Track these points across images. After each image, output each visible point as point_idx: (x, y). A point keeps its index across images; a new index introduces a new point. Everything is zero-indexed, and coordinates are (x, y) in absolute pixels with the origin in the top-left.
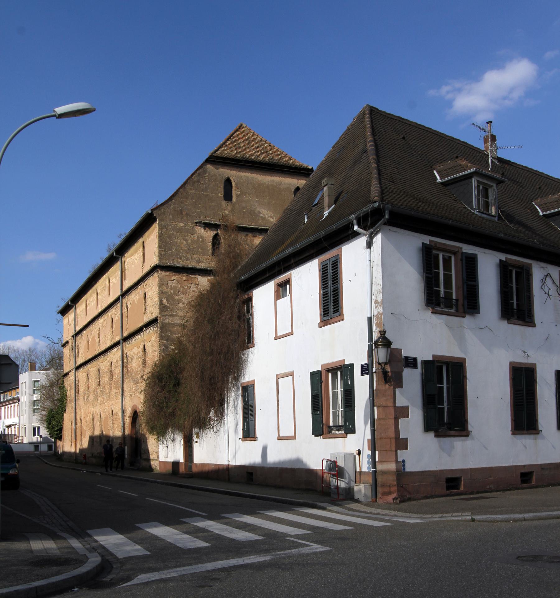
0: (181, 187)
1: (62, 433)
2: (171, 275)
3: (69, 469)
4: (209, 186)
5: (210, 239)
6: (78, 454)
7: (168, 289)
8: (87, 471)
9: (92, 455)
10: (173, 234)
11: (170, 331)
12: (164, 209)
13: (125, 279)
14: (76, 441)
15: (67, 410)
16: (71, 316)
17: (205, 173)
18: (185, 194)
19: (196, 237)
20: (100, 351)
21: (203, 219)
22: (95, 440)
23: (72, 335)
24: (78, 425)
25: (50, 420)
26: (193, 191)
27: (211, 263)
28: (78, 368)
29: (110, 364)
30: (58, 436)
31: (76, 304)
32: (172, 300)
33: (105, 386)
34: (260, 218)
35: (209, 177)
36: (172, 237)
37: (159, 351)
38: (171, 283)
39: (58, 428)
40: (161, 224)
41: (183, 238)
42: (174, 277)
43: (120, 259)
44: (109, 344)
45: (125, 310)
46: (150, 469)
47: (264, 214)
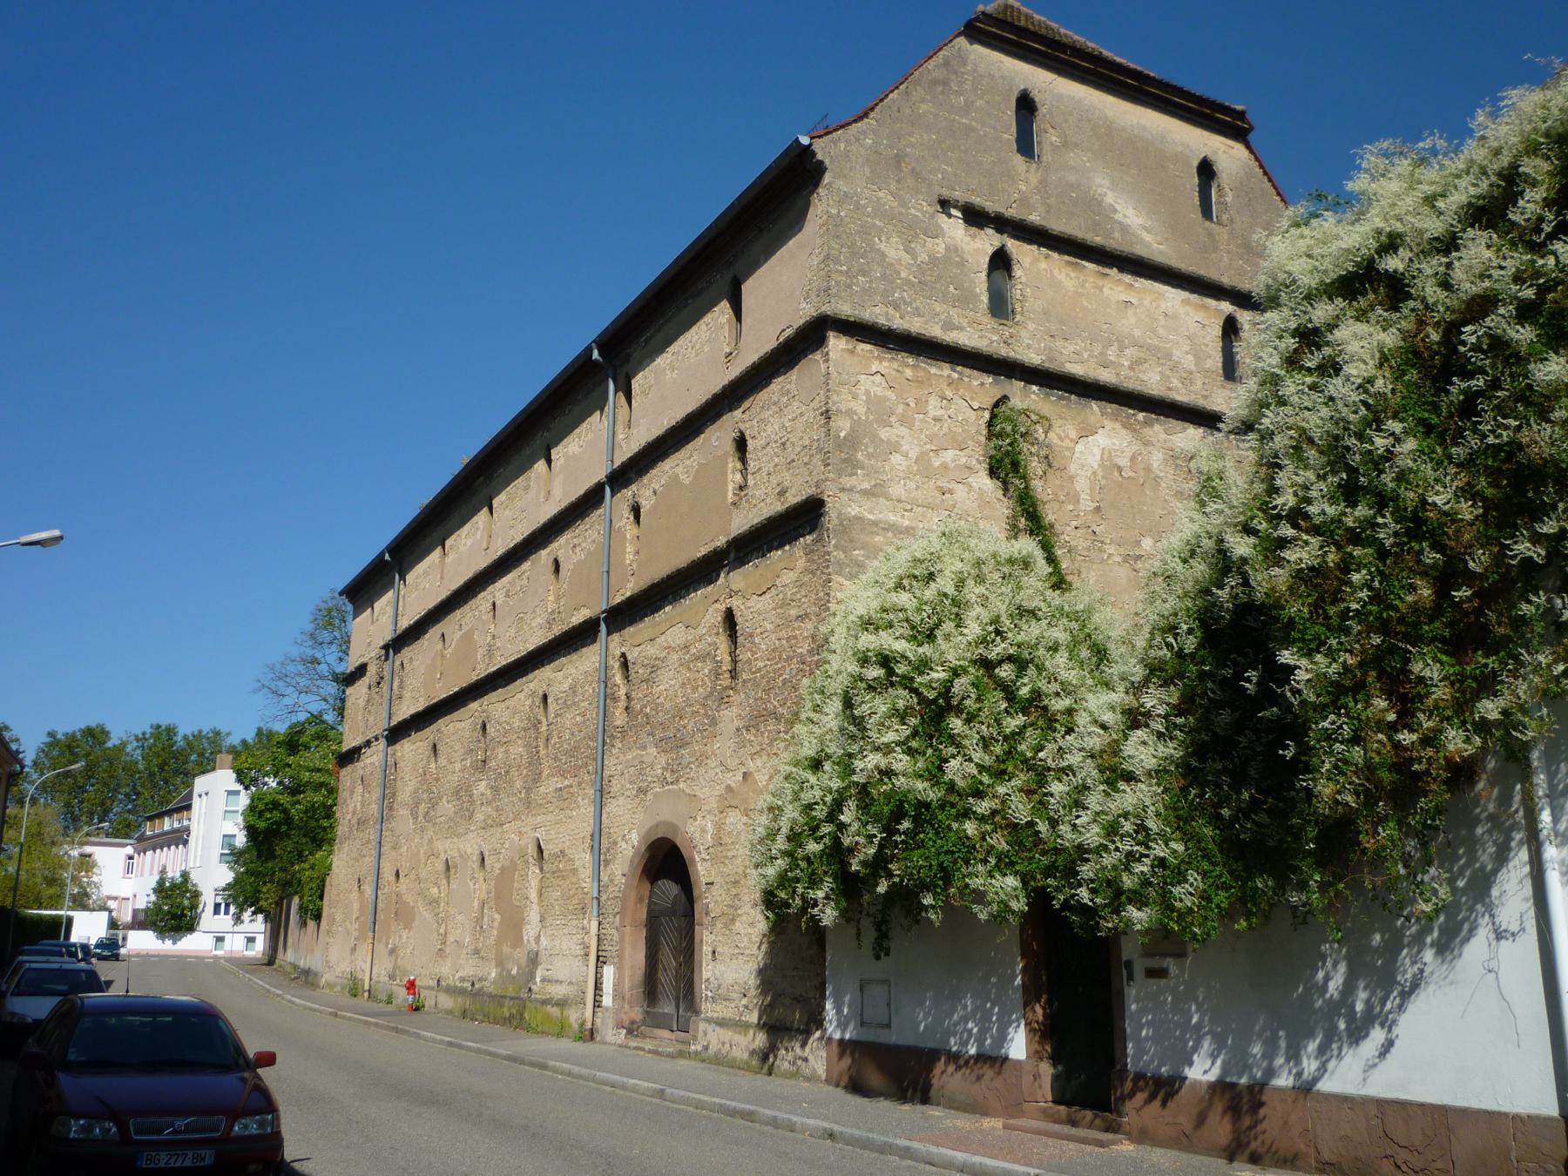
18: (907, 111)
21: (959, 195)
28: (397, 733)
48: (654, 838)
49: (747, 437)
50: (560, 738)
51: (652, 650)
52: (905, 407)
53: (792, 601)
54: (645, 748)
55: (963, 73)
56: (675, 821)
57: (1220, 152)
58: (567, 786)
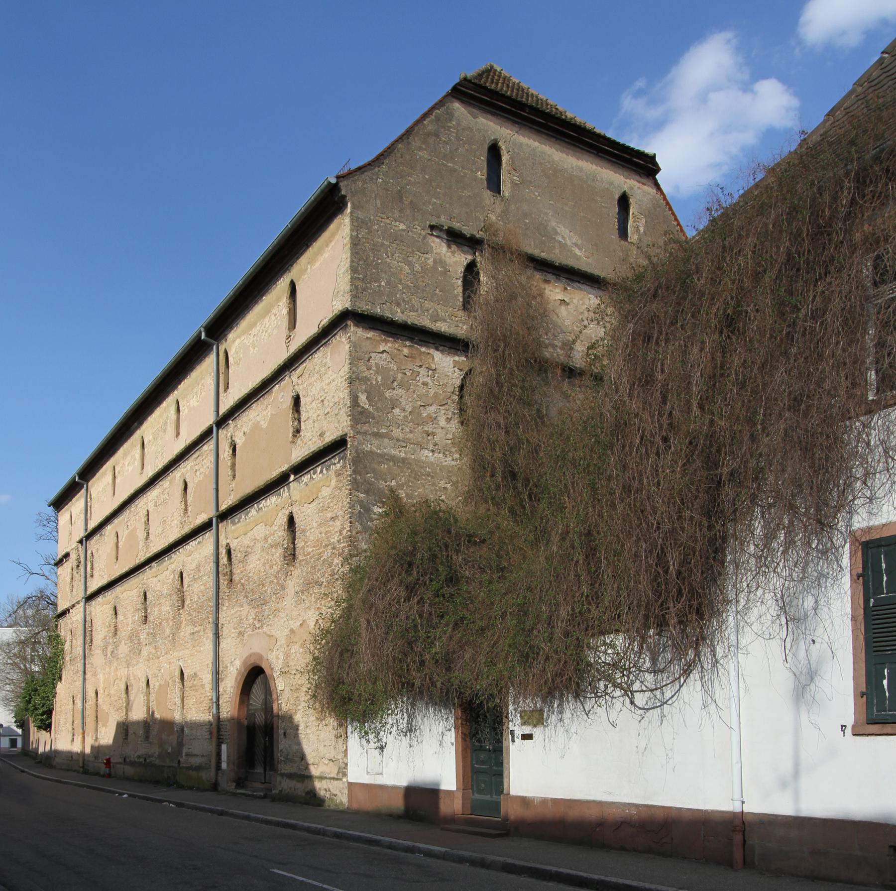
0: (400, 139)
1: (51, 718)
2: (378, 338)
3: (83, 786)
4: (457, 149)
5: (461, 270)
6: (89, 755)
7: (371, 372)
8: (130, 795)
9: (125, 759)
10: (383, 244)
11: (374, 471)
12: (364, 182)
13: (227, 387)
14: (84, 732)
15: (64, 677)
16: (77, 505)
17: (451, 120)
18: (408, 157)
19: (431, 262)
20: (148, 555)
21: (444, 221)
22: (131, 731)
23: (78, 539)
24: (90, 702)
25: (30, 695)
26: (424, 154)
27: (461, 325)
28: (90, 598)
29: (177, 576)
30: (44, 724)
31: (88, 481)
32: (380, 400)
33: (160, 623)
34: (557, 244)
35: (458, 131)
36: (379, 251)
37: (350, 517)
38: (376, 359)
39: (45, 709)
40: (356, 215)
41: (403, 258)
42: (384, 344)
43: (215, 347)
44: (174, 535)
45: (226, 453)
46: (313, 800)
47: (563, 237)
48: (249, 663)
49: (301, 396)
50: (191, 600)
51: (246, 541)
52: (403, 375)
53: (329, 507)
54: (242, 606)
55: (450, 127)
56: (261, 652)
57: (636, 188)
58: (197, 632)
